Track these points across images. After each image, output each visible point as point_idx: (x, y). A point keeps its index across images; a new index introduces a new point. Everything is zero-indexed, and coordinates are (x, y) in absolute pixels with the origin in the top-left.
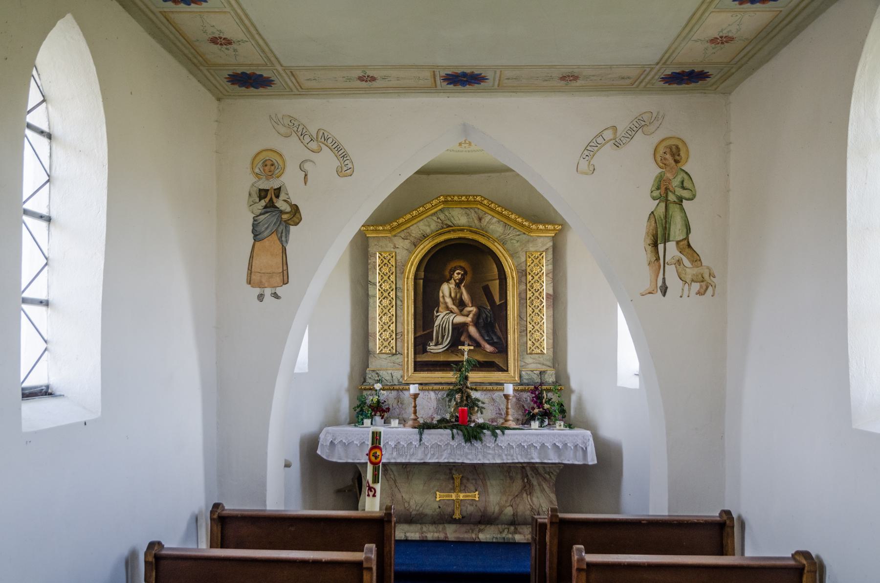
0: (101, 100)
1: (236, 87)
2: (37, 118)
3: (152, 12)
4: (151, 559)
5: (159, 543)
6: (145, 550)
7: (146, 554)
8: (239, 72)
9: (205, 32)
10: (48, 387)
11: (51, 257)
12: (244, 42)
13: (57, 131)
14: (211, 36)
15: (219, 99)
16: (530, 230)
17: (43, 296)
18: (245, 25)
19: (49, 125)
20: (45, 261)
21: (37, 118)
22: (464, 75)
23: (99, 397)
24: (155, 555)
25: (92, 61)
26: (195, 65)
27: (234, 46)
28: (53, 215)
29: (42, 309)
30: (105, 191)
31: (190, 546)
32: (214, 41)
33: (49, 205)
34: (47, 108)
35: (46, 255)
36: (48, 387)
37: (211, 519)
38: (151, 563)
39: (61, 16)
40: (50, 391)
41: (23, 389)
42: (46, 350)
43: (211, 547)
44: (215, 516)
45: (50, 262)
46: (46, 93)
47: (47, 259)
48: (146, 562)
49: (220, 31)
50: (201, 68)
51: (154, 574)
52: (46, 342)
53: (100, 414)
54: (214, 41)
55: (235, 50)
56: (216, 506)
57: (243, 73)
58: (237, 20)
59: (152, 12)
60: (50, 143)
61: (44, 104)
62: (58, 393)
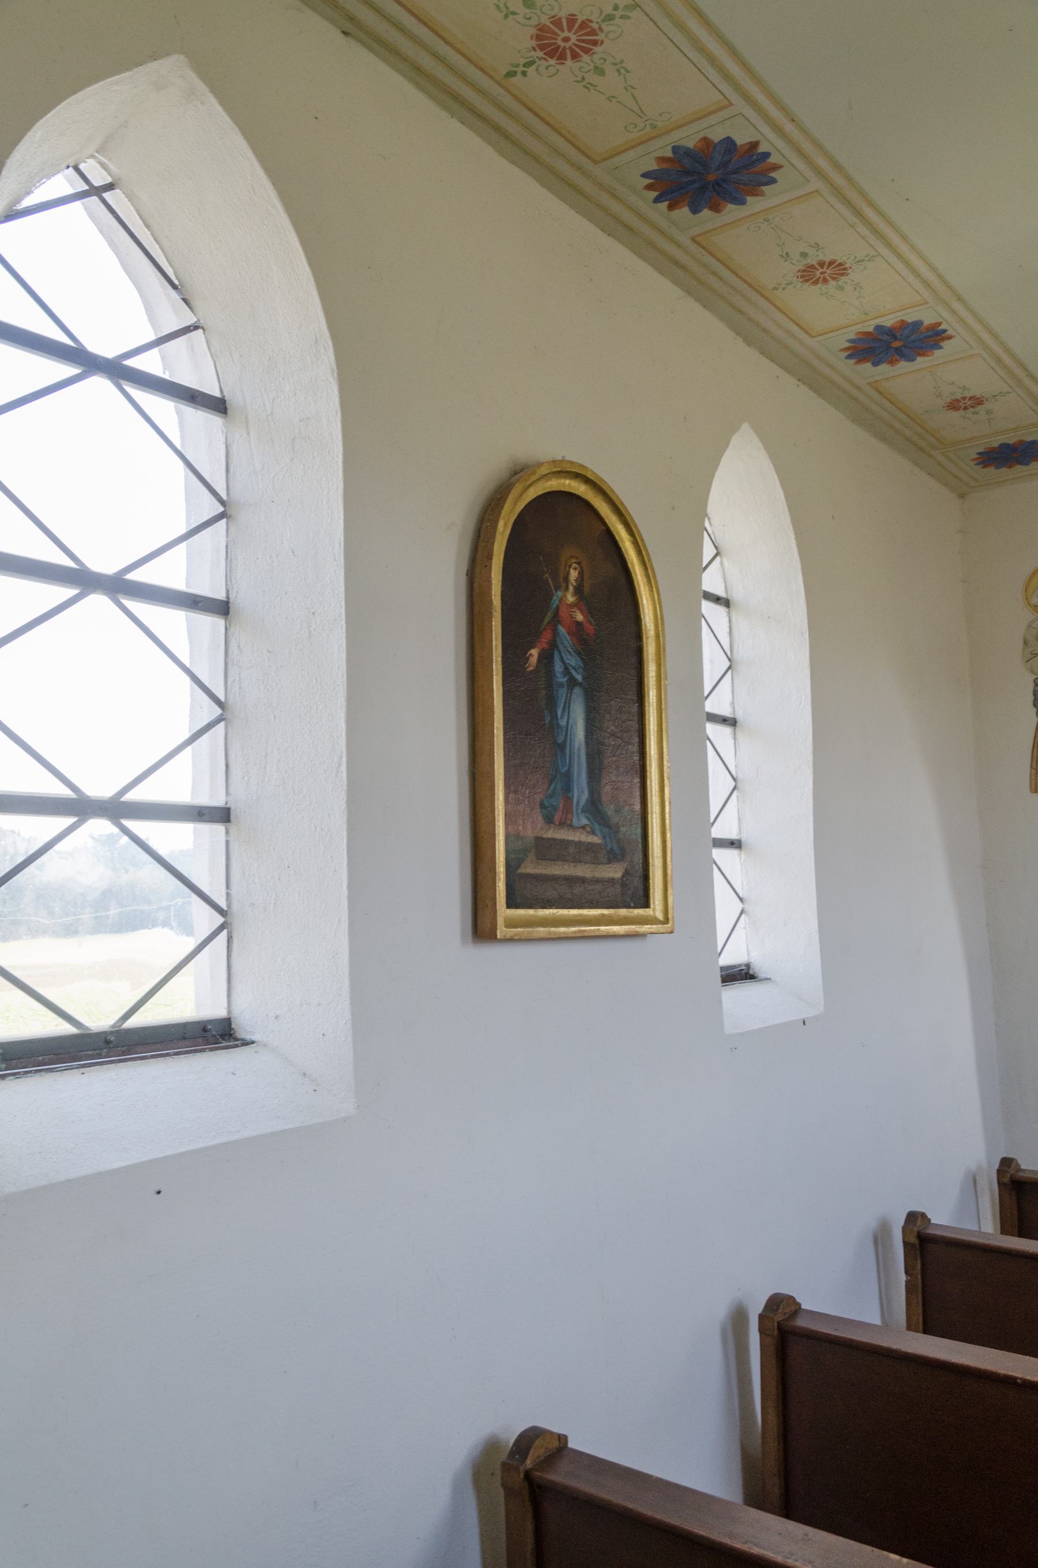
0: (793, 536)
1: (991, 470)
2: (711, 581)
3: (857, 388)
4: (913, 1239)
5: (923, 1215)
6: (902, 1223)
7: (904, 1230)
8: (995, 445)
9: (939, 396)
10: (748, 966)
11: (740, 776)
12: (1009, 393)
13: (737, 595)
14: (949, 400)
15: (962, 496)
16: (556, 614)
17: (733, 835)
18: (1005, 367)
19: (726, 587)
20: (733, 784)
21: (711, 581)
22: (891, 333)
23: (819, 982)
24: (918, 1232)
25: (778, 483)
26: (921, 449)
27: (987, 405)
28: (740, 716)
29: (733, 853)
30: (808, 672)
31: (968, 1226)
32: (954, 406)
33: (733, 703)
34: (722, 564)
35: (734, 774)
36: (748, 966)
37: (1000, 1184)
38: (913, 1245)
39: (734, 429)
40: (751, 972)
41: (722, 969)
42: (742, 912)
43: (1004, 1231)
44: (1006, 1180)
45: (739, 785)
46: (719, 542)
47: (734, 779)
48: (906, 1244)
49: (964, 388)
50: (933, 453)
51: (919, 1261)
52: (741, 899)
53: (822, 1008)
54: (954, 406)
55: (989, 412)
56: (1006, 1163)
57: (1003, 446)
58: (993, 364)
59: (857, 388)
60: (729, 613)
61: (718, 559)
62: (762, 976)
